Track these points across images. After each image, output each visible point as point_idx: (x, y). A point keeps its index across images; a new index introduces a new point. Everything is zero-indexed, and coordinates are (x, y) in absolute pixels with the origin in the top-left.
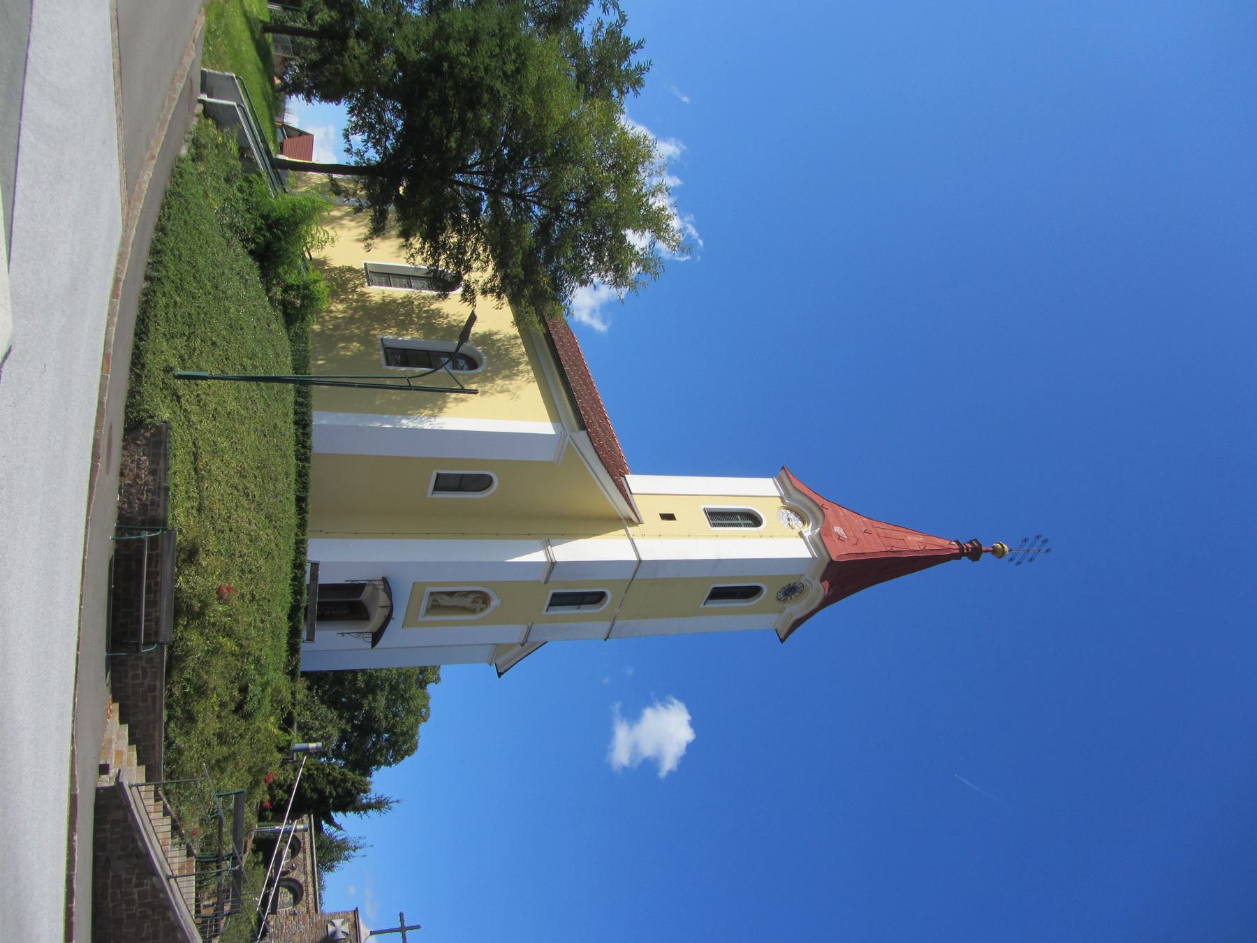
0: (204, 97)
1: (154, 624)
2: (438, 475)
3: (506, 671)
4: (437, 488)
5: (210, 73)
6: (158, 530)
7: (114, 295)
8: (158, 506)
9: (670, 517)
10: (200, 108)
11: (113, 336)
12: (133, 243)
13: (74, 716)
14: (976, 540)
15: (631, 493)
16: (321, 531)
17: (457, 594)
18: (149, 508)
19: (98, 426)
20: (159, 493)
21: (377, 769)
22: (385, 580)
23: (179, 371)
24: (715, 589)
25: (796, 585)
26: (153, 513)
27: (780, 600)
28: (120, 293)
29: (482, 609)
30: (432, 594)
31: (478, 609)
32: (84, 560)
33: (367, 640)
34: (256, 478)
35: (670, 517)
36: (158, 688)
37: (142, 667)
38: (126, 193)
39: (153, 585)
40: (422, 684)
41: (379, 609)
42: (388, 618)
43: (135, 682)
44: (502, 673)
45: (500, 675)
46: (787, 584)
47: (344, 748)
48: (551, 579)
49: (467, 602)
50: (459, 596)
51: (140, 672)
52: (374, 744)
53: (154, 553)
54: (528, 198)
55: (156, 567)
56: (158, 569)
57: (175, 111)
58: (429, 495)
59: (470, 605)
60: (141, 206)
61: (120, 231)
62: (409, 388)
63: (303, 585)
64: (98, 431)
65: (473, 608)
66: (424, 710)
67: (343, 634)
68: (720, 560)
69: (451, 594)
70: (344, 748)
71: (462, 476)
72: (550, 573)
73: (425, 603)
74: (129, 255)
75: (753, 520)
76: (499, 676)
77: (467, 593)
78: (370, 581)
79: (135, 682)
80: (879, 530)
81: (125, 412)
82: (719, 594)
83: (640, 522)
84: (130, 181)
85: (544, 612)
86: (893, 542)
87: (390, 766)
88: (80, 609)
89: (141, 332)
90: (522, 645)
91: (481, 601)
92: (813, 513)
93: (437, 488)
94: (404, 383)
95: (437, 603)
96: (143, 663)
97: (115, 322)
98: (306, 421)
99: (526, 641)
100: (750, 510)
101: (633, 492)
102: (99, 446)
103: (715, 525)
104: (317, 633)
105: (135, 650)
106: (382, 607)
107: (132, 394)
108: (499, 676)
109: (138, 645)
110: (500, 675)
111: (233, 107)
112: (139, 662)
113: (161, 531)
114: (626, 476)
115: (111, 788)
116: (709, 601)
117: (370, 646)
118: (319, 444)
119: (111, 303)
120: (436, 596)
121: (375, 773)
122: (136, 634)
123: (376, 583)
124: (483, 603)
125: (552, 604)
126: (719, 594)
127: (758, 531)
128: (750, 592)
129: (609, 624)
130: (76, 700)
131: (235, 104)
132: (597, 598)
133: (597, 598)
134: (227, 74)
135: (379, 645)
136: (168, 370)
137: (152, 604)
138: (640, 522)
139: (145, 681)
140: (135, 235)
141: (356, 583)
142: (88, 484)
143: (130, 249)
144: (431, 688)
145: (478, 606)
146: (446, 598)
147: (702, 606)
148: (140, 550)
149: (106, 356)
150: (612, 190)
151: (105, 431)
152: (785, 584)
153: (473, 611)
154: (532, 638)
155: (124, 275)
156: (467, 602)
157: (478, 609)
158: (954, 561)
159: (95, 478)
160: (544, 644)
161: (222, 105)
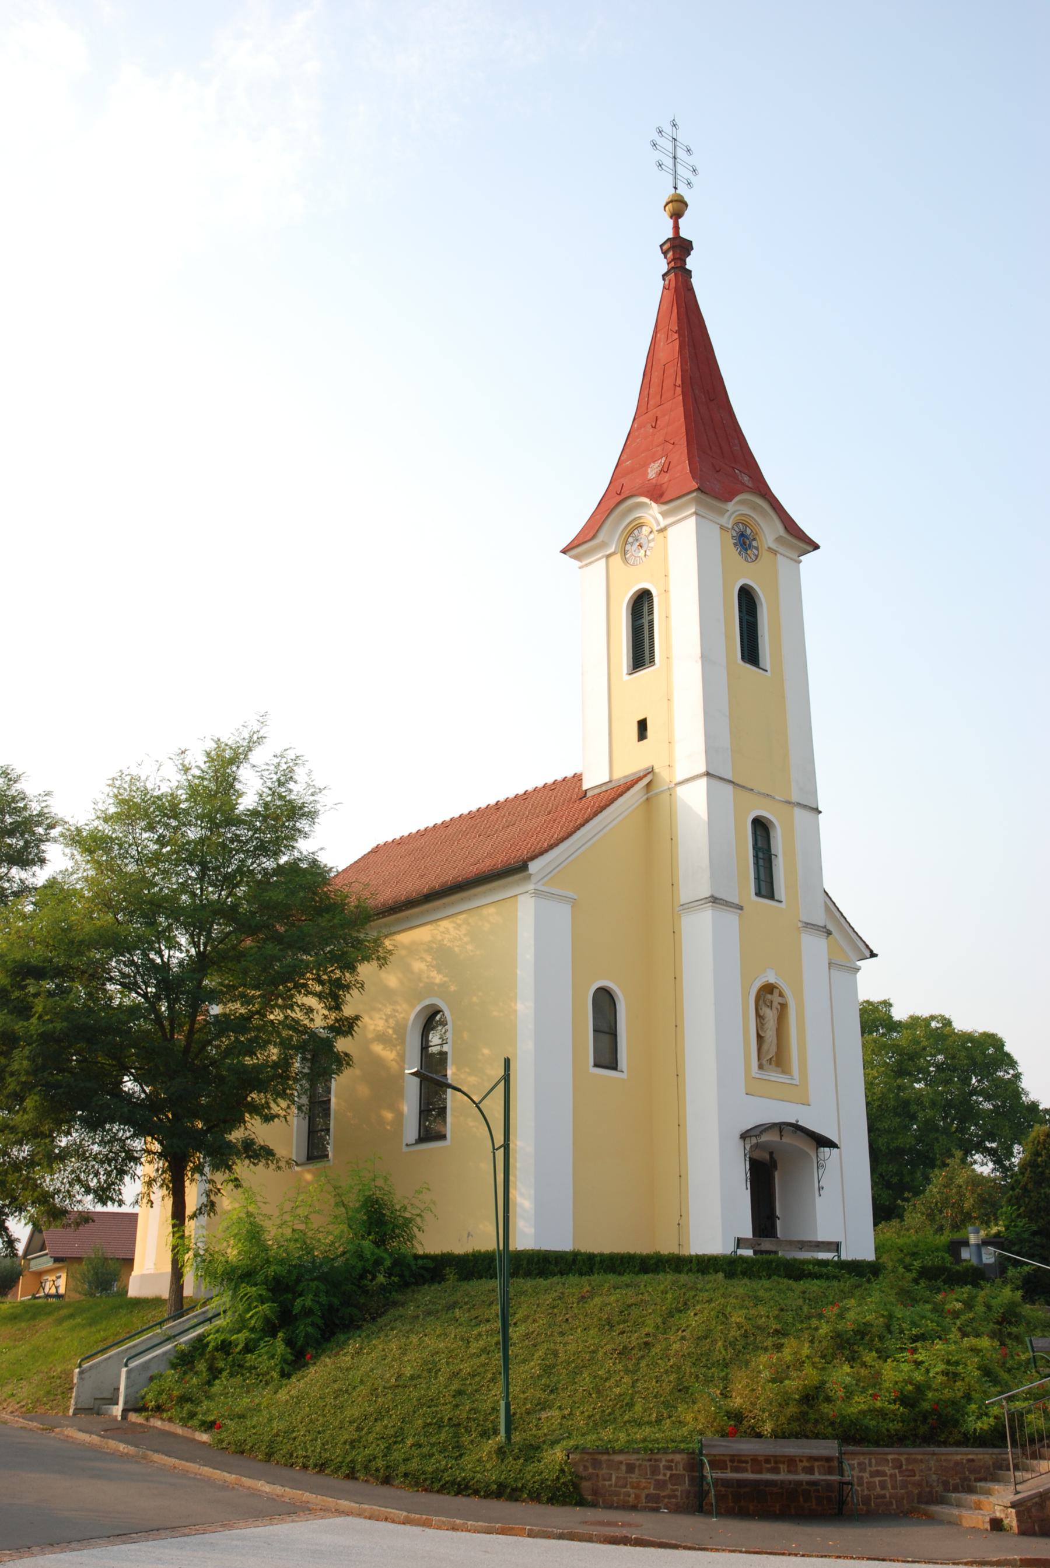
0: (117, 1410)
1: (816, 1464)
2: (596, 1065)
3: (867, 946)
4: (613, 1066)
5: (76, 1404)
6: (701, 1460)
7: (427, 1524)
8: (672, 1461)
9: (642, 725)
10: (133, 1417)
11: (480, 1523)
12: (357, 1503)
13: (929, 1562)
14: (661, 246)
15: (610, 781)
16: (679, 1224)
17: (760, 1032)
18: (674, 1472)
19: (589, 1539)
20: (656, 1460)
21: (1027, 1095)
22: (744, 1136)
23: (501, 1437)
24: (743, 658)
25: (735, 534)
26: (681, 1467)
27: (757, 556)
28: (424, 1517)
29: (781, 995)
30: (761, 1067)
31: (780, 1000)
32: (746, 1552)
33: (827, 1155)
34: (624, 1332)
35: (642, 725)
36: (896, 1456)
37: (871, 1477)
38: (302, 1514)
39: (768, 1466)
40: (893, 1026)
41: (784, 1140)
42: (797, 1128)
43: (889, 1486)
44: (871, 951)
45: (873, 955)
46: (734, 549)
47: (994, 1145)
48: (736, 902)
49: (770, 1015)
50: (762, 1029)
51: (877, 1479)
52: (988, 1098)
53: (729, 1464)
54: (202, 949)
55: (746, 1462)
56: (749, 1459)
57: (163, 1454)
58: (624, 1076)
59: (775, 1012)
60: (308, 1494)
61: (340, 1520)
62: (506, 1146)
63: (758, 1261)
64: (594, 1539)
65: (779, 1007)
66: (934, 1024)
67: (820, 1188)
68: (703, 657)
69: (760, 1038)
70: (994, 1145)
71: (595, 1031)
72: (727, 904)
73: (775, 1076)
74: (374, 1507)
75: (642, 603)
76: (876, 955)
77: (759, 1016)
78: (745, 1155)
79: (889, 1486)
80: (651, 403)
81: (485, 1497)
82: (751, 653)
83: (651, 771)
84: (293, 1510)
85: (783, 906)
86: (669, 383)
87: (1021, 1074)
88: (803, 1556)
89: (462, 1488)
90: (829, 933)
91: (769, 996)
92: (630, 510)
93: (613, 1066)
94: (500, 1153)
95: (774, 1059)
96: (866, 1475)
97: (462, 1522)
98: (539, 1260)
99: (825, 927)
100: (631, 598)
101: (607, 780)
102: (613, 1537)
103: (652, 661)
104: (822, 1237)
105: (850, 1486)
106: (781, 1136)
107: (535, 1497)
108: (876, 955)
109: (842, 1484)
110: (873, 955)
111: (129, 1372)
112: (865, 1480)
113: (703, 1458)
114: (585, 788)
115: (1018, 1514)
116: (761, 665)
117: (836, 1149)
118: (562, 1242)
119: (439, 1528)
120: (764, 1062)
121: (1033, 1096)
122: (829, 1485)
123: (748, 1147)
124: (771, 993)
125: (771, 896)
126: (751, 653)
127: (658, 595)
128: (747, 600)
129: (797, 811)
130: (910, 1559)
131: (124, 1370)
132: (761, 827)
133: (761, 827)
134: (75, 1381)
135: (834, 1138)
136: (501, 1452)
137: (791, 1462)
138: (651, 771)
139: (889, 1473)
140: (346, 1500)
141: (749, 1175)
142: (659, 1550)
143: (366, 1506)
144: (899, 1014)
145: (776, 999)
146: (765, 1047)
147: (769, 674)
148: (726, 1483)
149: (503, 1532)
150: (341, 993)
151: (595, 1530)
152: (734, 552)
153: (783, 1006)
154: (820, 919)
155: (401, 1512)
156: (770, 1015)
157: (780, 1000)
158: (693, 280)
159: (649, 1540)
160: (827, 894)
161: (127, 1387)
